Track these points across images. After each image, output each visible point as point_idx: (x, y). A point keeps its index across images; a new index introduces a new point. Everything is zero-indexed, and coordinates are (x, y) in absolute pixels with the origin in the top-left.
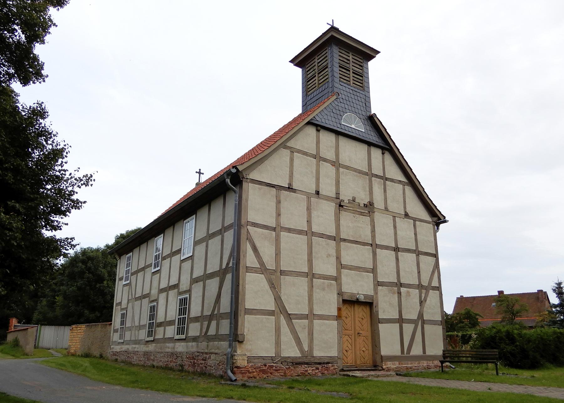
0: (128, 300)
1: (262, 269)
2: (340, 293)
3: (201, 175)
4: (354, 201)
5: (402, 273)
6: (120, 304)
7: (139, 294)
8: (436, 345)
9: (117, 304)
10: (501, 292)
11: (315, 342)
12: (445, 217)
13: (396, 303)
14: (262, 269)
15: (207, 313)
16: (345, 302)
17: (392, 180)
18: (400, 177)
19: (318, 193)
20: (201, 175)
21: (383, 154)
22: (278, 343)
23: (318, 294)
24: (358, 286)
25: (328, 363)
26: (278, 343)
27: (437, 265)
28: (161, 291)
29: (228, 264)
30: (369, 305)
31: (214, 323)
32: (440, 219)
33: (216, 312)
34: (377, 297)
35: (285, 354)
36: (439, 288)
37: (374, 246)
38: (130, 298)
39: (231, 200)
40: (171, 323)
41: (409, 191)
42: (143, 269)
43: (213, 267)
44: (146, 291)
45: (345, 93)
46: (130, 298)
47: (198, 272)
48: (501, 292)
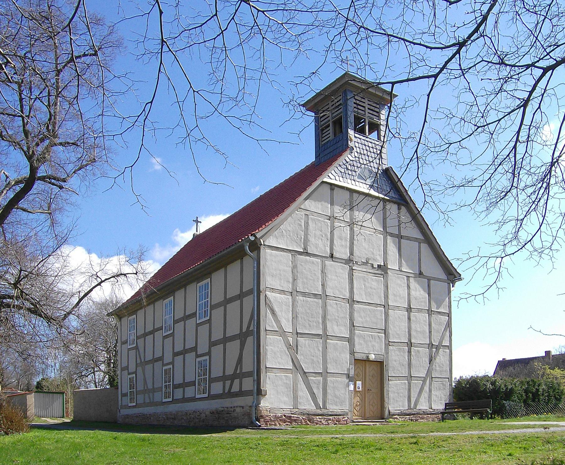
0: (137, 364)
1: (282, 333)
2: (352, 353)
3: (199, 224)
4: (367, 262)
5: (413, 333)
6: (127, 368)
7: (149, 357)
8: (439, 400)
9: (123, 369)
10: (548, 353)
11: (329, 397)
12: (460, 275)
13: (406, 363)
14: (282, 333)
15: (230, 371)
16: (357, 361)
17: (408, 238)
18: (417, 234)
19: (332, 256)
20: (199, 224)
21: (399, 209)
22: (295, 398)
23: (331, 354)
24: (370, 348)
25: (340, 415)
26: (295, 398)
27: (449, 325)
28: (176, 354)
29: (248, 327)
30: (380, 365)
31: (237, 382)
32: (455, 277)
33: (238, 372)
34: (387, 357)
35: (301, 407)
36: (450, 347)
37: (387, 307)
38: (139, 361)
39: (248, 262)
40: (193, 383)
41: (425, 247)
42: (152, 332)
43: (233, 329)
44: (158, 354)
45: (360, 146)
46: (139, 361)
47: (217, 335)
48: (548, 353)
